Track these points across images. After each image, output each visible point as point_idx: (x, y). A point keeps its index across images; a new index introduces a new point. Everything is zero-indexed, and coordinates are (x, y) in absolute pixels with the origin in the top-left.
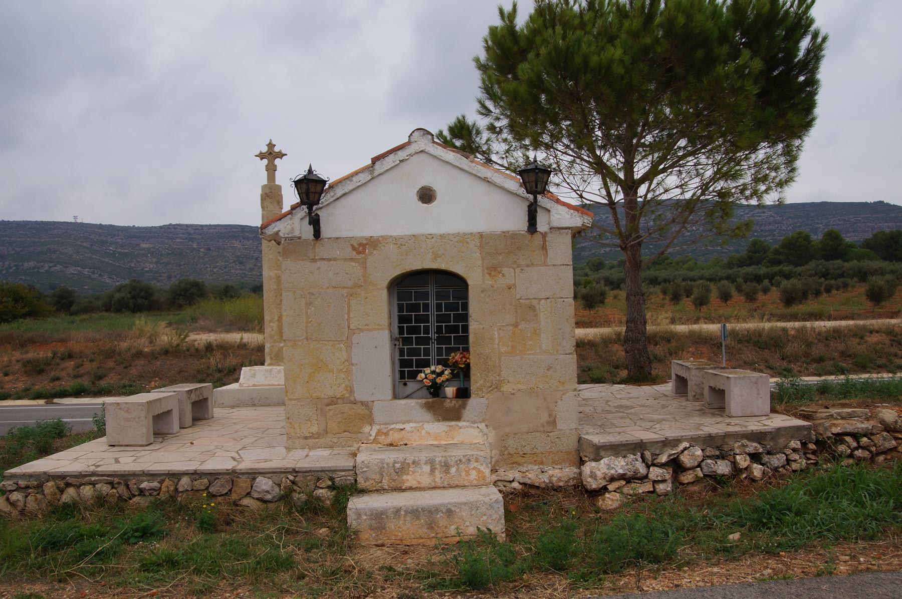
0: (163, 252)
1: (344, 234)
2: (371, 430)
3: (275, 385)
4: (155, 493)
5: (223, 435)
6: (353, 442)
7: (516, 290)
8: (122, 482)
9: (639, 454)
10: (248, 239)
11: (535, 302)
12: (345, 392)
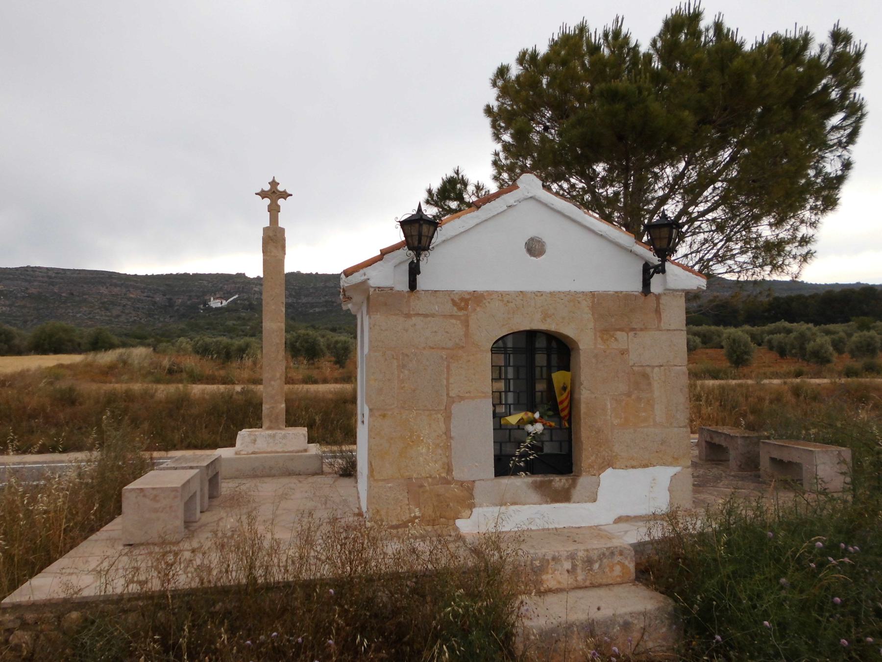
0: (19, 295)
7: (629, 356)
10: (116, 285)
11: (648, 370)
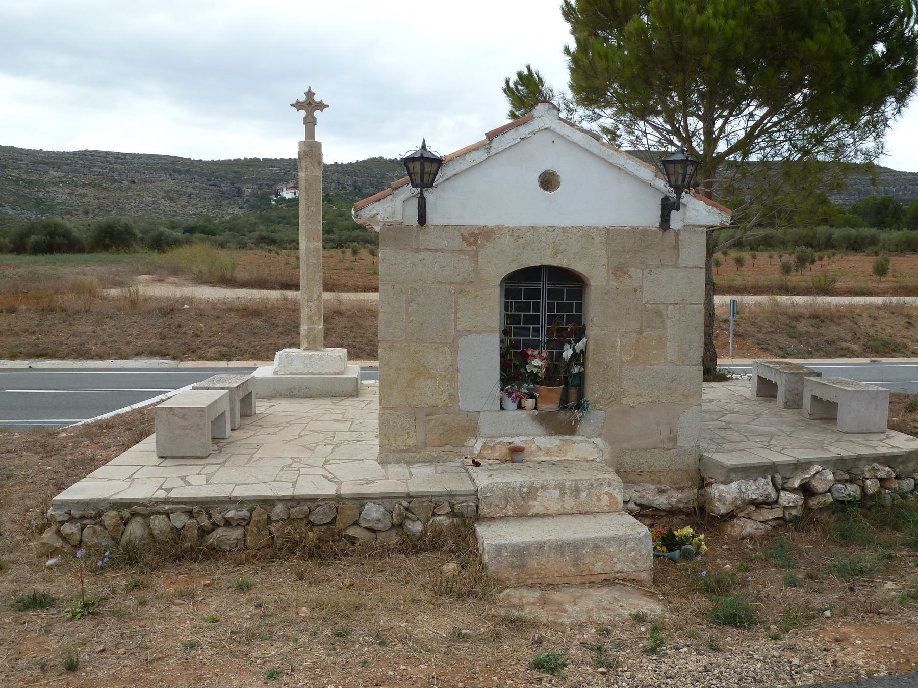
0: (79, 183)
1: (453, 222)
2: (476, 443)
3: (315, 374)
4: (244, 523)
5: (290, 441)
6: (455, 456)
7: (642, 293)
8: (203, 510)
9: (769, 477)
11: (662, 307)
12: (447, 401)
